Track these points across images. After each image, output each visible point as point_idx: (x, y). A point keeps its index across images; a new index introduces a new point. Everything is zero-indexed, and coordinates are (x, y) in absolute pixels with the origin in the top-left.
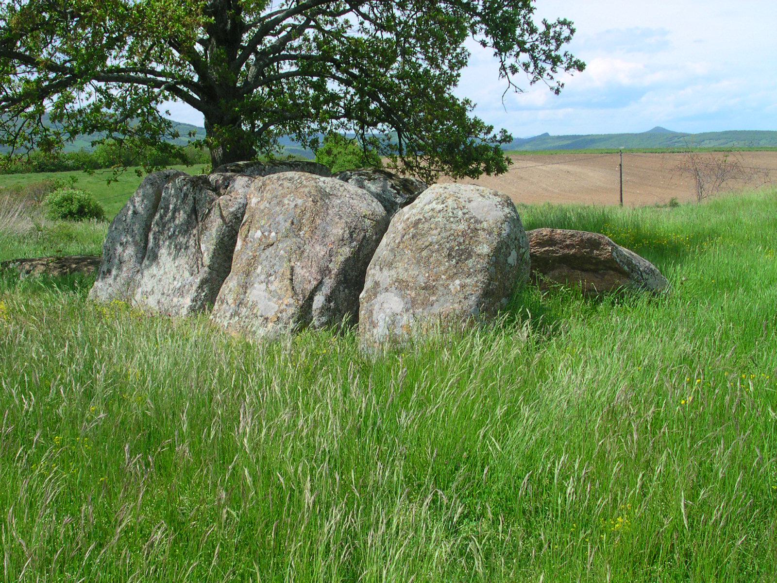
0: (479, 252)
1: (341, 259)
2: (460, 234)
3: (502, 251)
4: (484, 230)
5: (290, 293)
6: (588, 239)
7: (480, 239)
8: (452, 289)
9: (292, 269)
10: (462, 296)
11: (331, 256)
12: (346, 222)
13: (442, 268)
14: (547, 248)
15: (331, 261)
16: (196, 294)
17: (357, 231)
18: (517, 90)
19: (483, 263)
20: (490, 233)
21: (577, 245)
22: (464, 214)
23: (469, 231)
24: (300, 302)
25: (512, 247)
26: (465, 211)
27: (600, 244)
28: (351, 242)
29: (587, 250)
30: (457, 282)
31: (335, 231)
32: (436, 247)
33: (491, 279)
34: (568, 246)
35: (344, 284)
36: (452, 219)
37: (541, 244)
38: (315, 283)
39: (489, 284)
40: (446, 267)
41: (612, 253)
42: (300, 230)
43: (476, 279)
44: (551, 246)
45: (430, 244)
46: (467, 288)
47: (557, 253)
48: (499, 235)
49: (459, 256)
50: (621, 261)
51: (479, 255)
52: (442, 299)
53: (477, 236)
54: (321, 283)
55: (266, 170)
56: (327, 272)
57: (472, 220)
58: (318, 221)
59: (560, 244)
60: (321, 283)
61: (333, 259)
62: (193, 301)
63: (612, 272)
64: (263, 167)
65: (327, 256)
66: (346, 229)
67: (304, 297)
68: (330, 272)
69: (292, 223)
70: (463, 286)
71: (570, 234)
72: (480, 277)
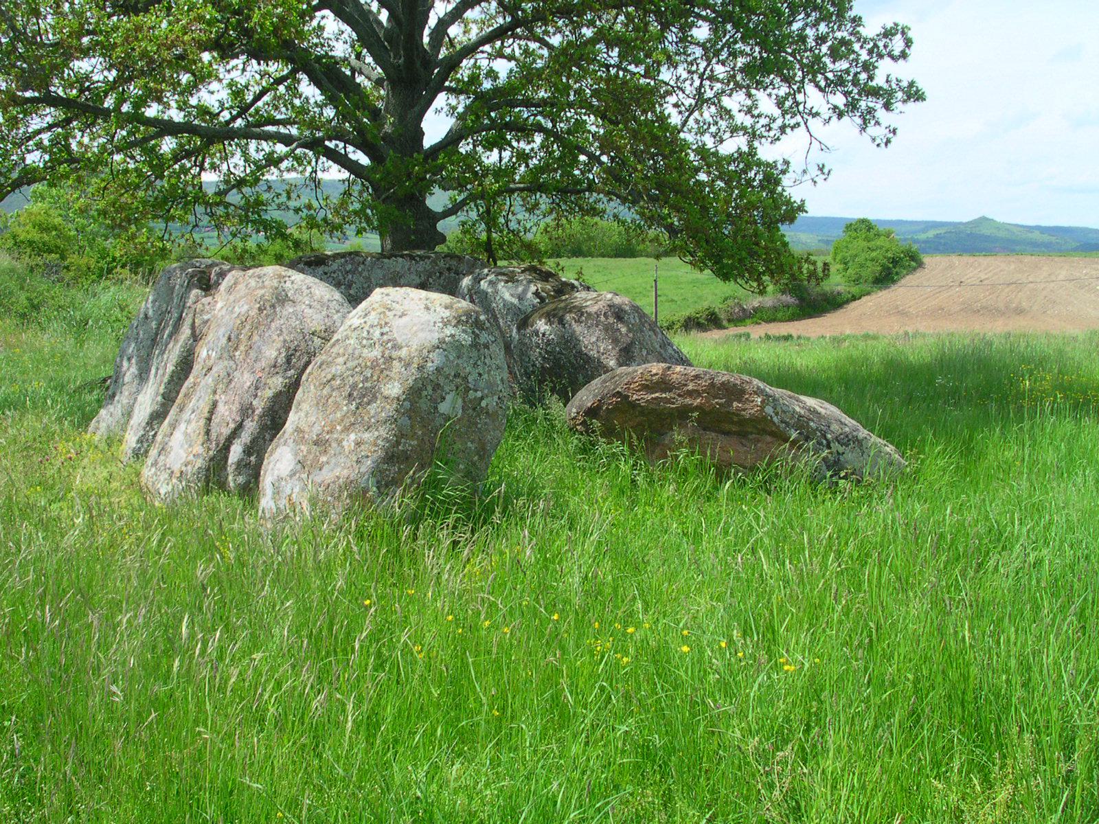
0: (386, 393)
1: (269, 393)
2: (369, 364)
3: (425, 393)
4: (400, 359)
5: (201, 439)
6: (723, 384)
7: (392, 375)
9: (215, 405)
10: (355, 459)
11: (257, 388)
12: (285, 341)
13: (339, 415)
14: (657, 395)
15: (256, 396)
16: (142, 432)
17: (298, 354)
18: (823, 147)
19: (390, 409)
20: (407, 365)
21: (704, 391)
22: (382, 334)
23: (382, 360)
24: (211, 453)
25: (447, 388)
26: (386, 330)
27: (743, 392)
28: (286, 370)
29: (720, 401)
30: (353, 436)
31: (268, 353)
32: (338, 382)
33: (401, 435)
34: (690, 393)
35: (270, 429)
36: (365, 342)
37: (647, 388)
38: (232, 426)
39: (398, 443)
40: (343, 413)
41: (762, 408)
42: (236, 349)
43: (376, 433)
44: (663, 391)
45: (333, 378)
46: (363, 447)
47: (673, 403)
48: (421, 368)
49: (360, 398)
51: (386, 398)
52: (333, 461)
53: (389, 369)
54: (240, 427)
55: (367, 263)
56: (250, 412)
57: (389, 345)
58: (256, 338)
59: (678, 389)
60: (240, 427)
61: (259, 394)
62: (138, 442)
63: (769, 438)
64: (361, 259)
65: (253, 388)
66: (283, 350)
67: (217, 445)
68: (253, 412)
69: (229, 339)
70: (358, 444)
71: (693, 373)
72: (383, 432)
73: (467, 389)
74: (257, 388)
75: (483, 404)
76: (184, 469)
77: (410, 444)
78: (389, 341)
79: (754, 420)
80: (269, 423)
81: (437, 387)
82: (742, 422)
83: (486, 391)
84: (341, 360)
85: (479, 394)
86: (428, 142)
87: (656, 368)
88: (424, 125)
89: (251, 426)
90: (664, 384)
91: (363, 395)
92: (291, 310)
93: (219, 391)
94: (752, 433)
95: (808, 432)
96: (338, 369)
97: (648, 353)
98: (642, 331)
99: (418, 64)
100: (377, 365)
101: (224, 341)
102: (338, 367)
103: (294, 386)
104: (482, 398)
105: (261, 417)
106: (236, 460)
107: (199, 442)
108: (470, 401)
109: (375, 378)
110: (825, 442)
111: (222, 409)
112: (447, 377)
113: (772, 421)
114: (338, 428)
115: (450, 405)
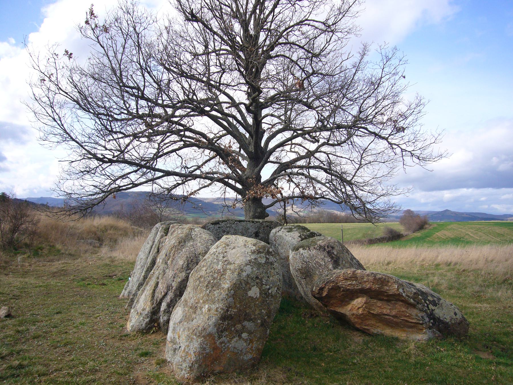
8: (204, 311)
9: (157, 284)
11: (174, 278)
19: (224, 295)
28: (187, 270)
33: (229, 307)
38: (163, 294)
39: (227, 311)
41: (398, 289)
42: (168, 259)
50: (407, 296)
53: (225, 274)
54: (166, 294)
56: (171, 288)
60: (166, 294)
63: (401, 303)
65: (173, 277)
69: (166, 255)
70: (209, 310)
73: (262, 284)
74: (174, 278)
75: (270, 291)
76: (142, 312)
77: (233, 311)
78: (226, 261)
79: (394, 295)
80: (178, 293)
81: (247, 283)
82: (388, 296)
83: (271, 285)
84: (205, 268)
85: (268, 287)
86: (263, 180)
87: (350, 271)
88: (261, 174)
89: (170, 295)
90: (354, 277)
91: (213, 285)
92: (192, 243)
93: (160, 278)
94: (393, 300)
95: (418, 300)
96: (203, 273)
97: (346, 263)
98: (343, 253)
99: (259, 152)
100: (220, 272)
101: (164, 256)
102: (203, 272)
103: (187, 279)
104: (269, 289)
105: (175, 290)
106: (163, 309)
107: (149, 301)
108: (263, 290)
109: (218, 278)
110: (426, 305)
111: (160, 285)
112: (252, 279)
113: (402, 295)
114: (201, 301)
115: (254, 292)
